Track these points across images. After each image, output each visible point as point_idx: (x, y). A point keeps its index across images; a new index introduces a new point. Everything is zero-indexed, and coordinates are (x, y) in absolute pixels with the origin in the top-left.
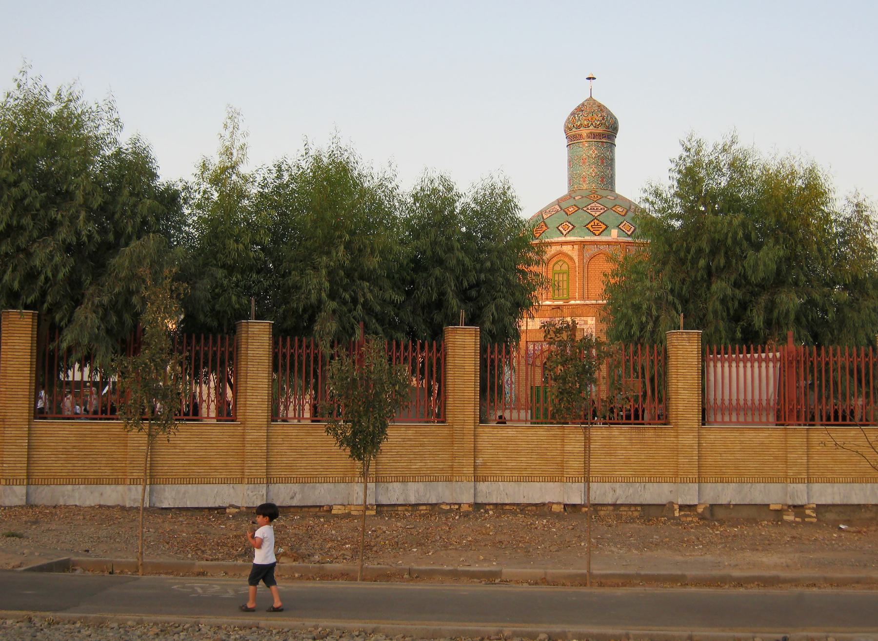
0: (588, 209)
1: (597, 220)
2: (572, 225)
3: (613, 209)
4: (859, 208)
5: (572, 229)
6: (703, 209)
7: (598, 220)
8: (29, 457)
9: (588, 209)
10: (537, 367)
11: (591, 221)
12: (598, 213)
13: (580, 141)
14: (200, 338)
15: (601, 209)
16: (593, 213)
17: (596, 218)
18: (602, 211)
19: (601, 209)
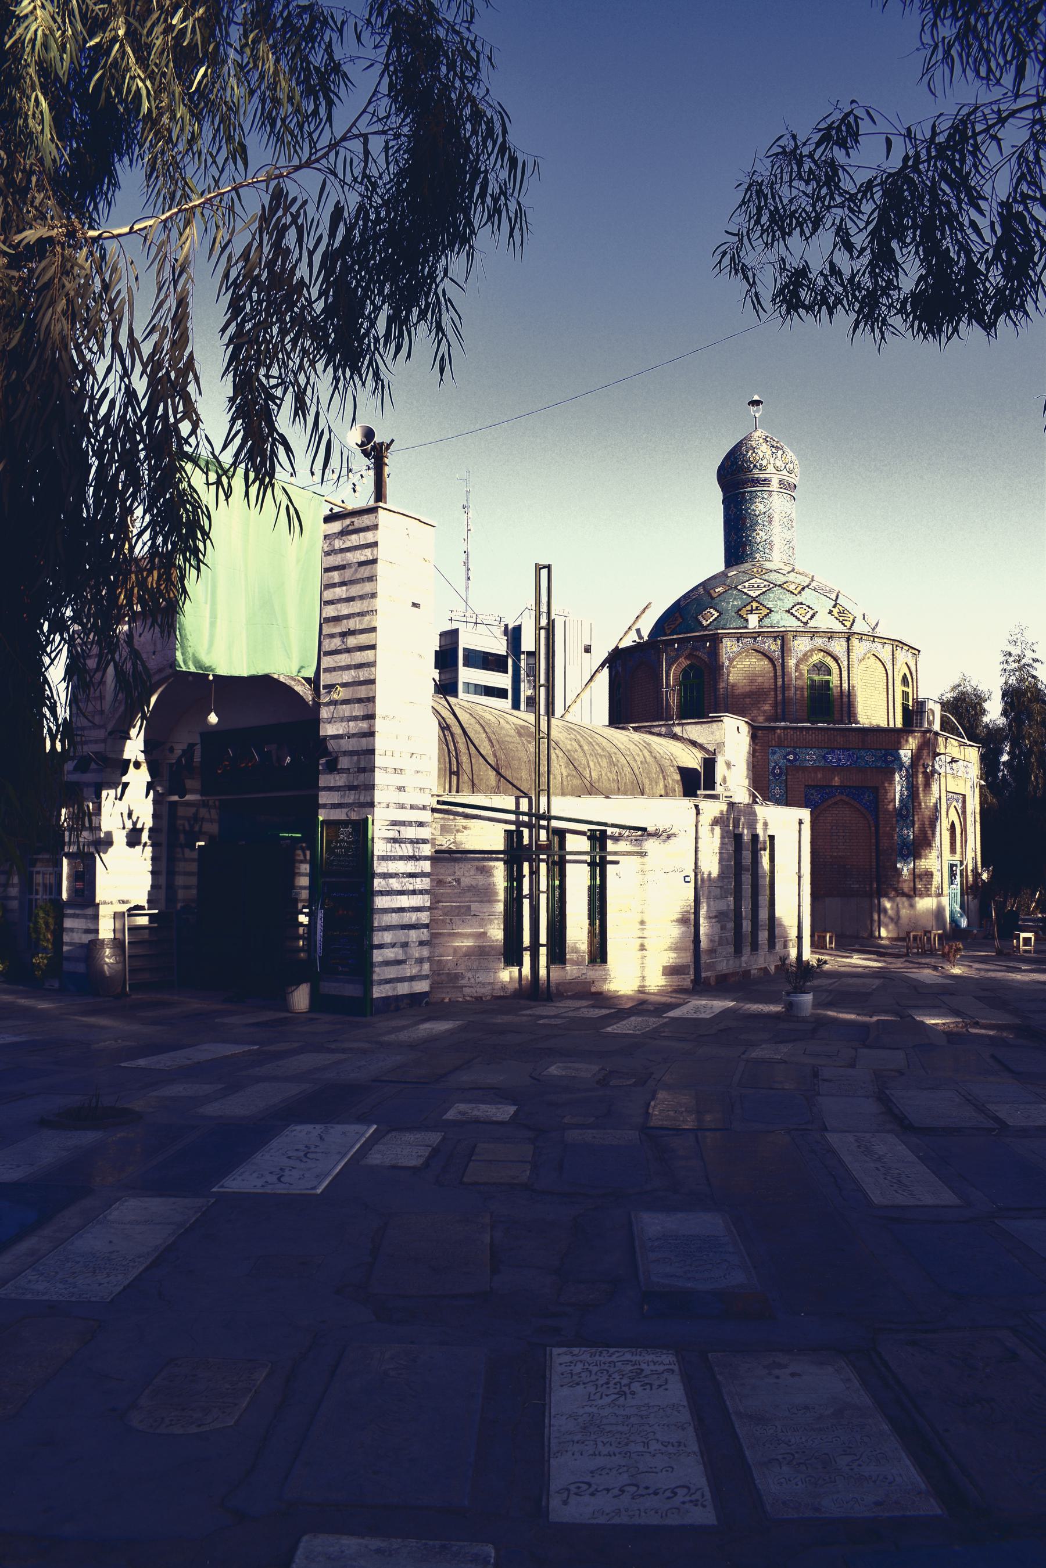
0: (745, 587)
1: (757, 601)
2: (792, 614)
3: (772, 586)
4: (670, 949)
5: (740, 610)
6: (139, 609)
7: (759, 603)
8: (645, 609)
9: (745, 587)
10: (233, 25)
11: (747, 605)
12: (758, 593)
13: (765, 489)
14: (188, 357)
15: (765, 586)
16: (751, 593)
17: (754, 599)
18: (764, 589)
19: (765, 586)
